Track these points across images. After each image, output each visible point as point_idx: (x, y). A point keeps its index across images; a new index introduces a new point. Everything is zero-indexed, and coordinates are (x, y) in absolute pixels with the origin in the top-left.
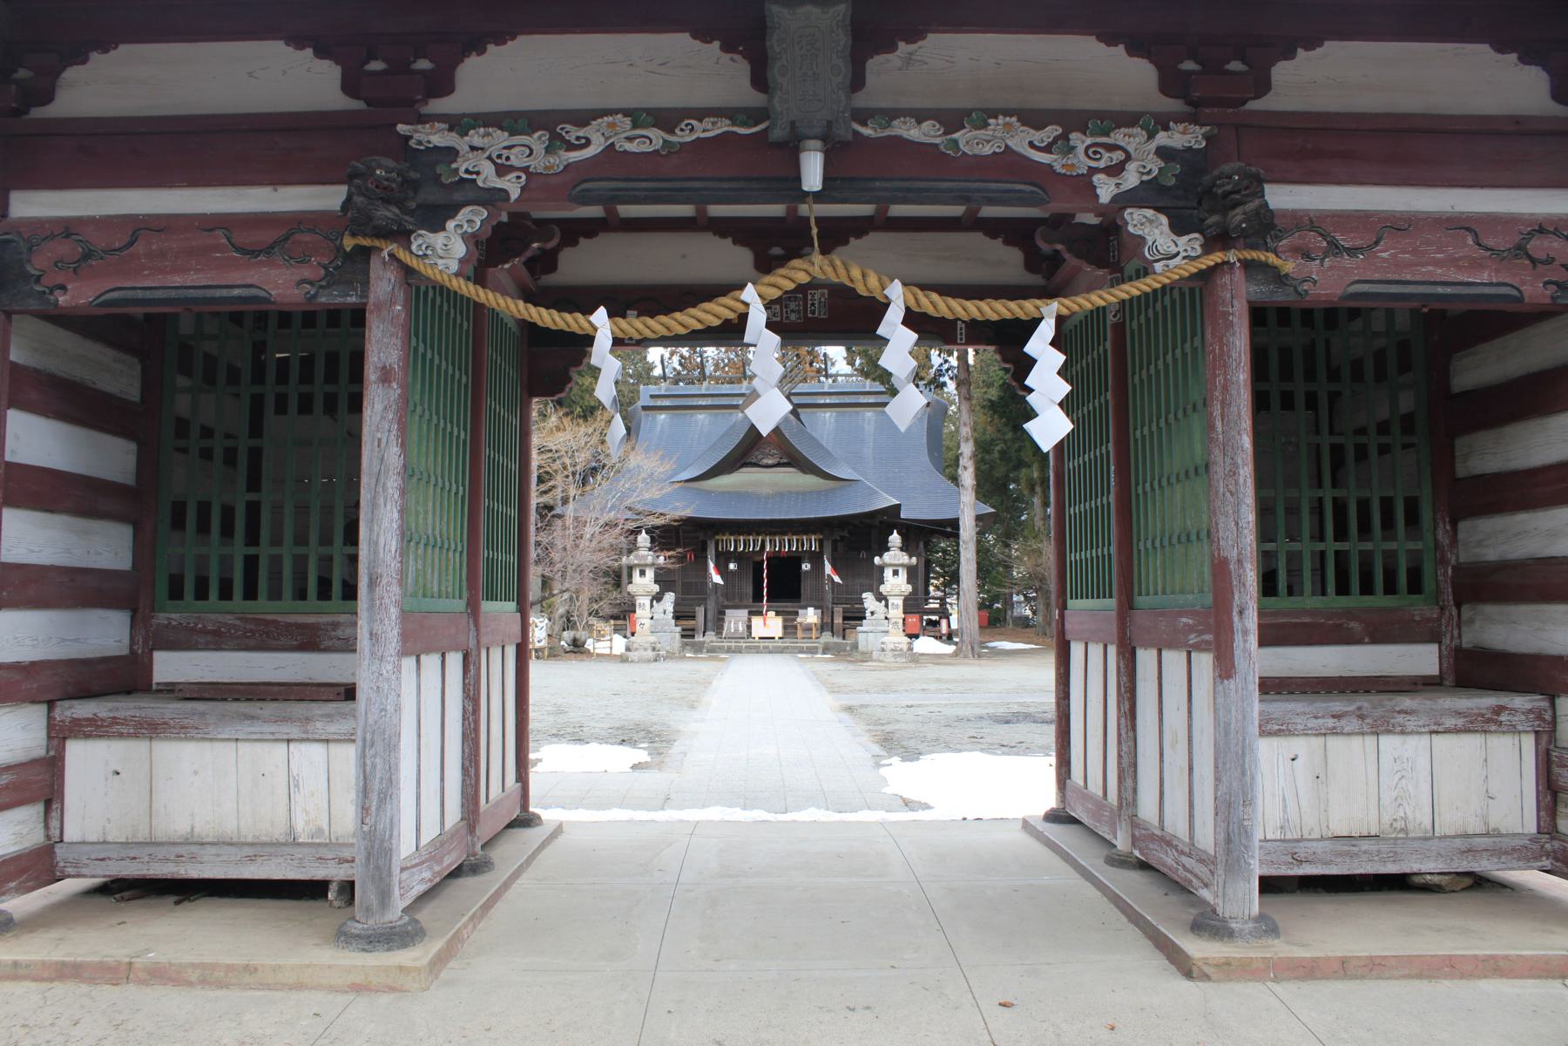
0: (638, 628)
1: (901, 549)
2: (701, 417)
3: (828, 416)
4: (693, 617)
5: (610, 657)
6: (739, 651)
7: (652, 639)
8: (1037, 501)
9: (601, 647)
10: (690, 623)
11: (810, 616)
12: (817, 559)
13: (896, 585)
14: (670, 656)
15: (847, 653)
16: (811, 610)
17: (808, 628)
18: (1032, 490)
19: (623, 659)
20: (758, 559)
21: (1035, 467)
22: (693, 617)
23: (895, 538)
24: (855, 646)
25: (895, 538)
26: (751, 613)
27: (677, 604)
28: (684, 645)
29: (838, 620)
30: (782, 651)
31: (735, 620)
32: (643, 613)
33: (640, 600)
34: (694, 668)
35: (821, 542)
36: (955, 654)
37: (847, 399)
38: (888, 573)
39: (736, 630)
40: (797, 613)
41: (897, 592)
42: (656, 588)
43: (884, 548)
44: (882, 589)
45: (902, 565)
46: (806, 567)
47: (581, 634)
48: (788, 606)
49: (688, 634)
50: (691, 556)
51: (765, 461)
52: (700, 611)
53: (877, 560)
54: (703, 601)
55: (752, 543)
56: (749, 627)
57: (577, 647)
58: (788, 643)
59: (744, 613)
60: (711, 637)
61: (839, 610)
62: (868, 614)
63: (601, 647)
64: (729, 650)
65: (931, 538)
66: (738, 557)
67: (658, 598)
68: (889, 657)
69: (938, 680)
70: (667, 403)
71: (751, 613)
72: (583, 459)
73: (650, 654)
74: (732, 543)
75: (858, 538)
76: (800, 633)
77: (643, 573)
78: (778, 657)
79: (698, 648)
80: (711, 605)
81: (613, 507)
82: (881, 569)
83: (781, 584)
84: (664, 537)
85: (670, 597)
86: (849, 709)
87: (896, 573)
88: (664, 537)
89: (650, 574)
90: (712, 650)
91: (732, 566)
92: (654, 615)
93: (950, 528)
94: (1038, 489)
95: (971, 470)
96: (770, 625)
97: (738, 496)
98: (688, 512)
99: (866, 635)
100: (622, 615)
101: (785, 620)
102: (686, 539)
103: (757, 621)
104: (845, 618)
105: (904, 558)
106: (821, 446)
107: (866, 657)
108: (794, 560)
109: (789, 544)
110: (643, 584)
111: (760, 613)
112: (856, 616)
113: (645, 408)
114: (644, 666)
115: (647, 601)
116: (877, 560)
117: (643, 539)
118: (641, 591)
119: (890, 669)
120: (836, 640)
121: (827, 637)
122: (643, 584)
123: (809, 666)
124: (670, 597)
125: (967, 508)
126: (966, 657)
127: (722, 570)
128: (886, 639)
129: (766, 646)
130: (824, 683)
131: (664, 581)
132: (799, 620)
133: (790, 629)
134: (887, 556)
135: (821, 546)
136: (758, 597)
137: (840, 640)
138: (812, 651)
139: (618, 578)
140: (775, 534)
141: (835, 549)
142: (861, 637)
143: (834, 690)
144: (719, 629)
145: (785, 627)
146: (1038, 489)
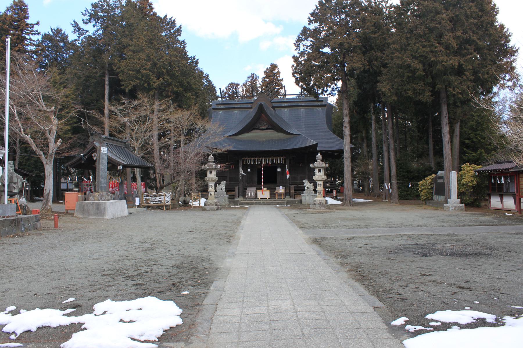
0: (209, 196)
1: (322, 161)
2: (236, 112)
3: (286, 110)
4: (234, 191)
5: (199, 208)
6: (252, 204)
7: (216, 200)
8: (364, 145)
9: (196, 203)
10: (232, 193)
11: (281, 190)
12: (283, 167)
13: (320, 176)
14: (224, 207)
15: (299, 205)
16: (281, 187)
17: (280, 194)
18: (363, 140)
19: (203, 209)
20: (259, 167)
21: (364, 132)
22: (234, 191)
23: (319, 156)
24: (301, 201)
25: (319, 156)
26: (257, 189)
27: (227, 185)
28: (230, 203)
29: (292, 191)
30: (270, 204)
31: (251, 192)
32: (211, 190)
33: (210, 184)
34: (235, 213)
35: (285, 160)
36: (342, 205)
37: (294, 104)
38: (316, 171)
39: (251, 196)
40: (275, 189)
41: (320, 179)
42: (217, 179)
43: (314, 160)
44: (314, 178)
45: (322, 167)
46: (279, 170)
47: (187, 198)
48: (272, 186)
49: (231, 197)
50: (232, 167)
51: (262, 128)
52: (236, 188)
53: (311, 165)
54: (238, 184)
55: (256, 161)
56: (256, 194)
57: (186, 204)
58: (272, 200)
59: (254, 189)
60: (241, 199)
61: (292, 187)
62: (306, 189)
63: (196, 203)
64: (248, 204)
65: (333, 157)
66: (251, 166)
67: (218, 183)
68: (318, 207)
69: (346, 219)
70: (222, 107)
71: (257, 189)
72: (186, 125)
73: (215, 207)
74: (250, 161)
75: (301, 160)
76: (277, 197)
77: (211, 173)
78: (269, 206)
79: (236, 203)
80: (241, 186)
81: (199, 146)
82: (313, 169)
83: (270, 179)
84: (220, 158)
85: (223, 183)
86: (316, 241)
87: (320, 171)
88: (220, 158)
89: (214, 173)
90: (242, 204)
91: (249, 170)
92: (217, 190)
93: (341, 152)
94: (365, 140)
95: (348, 128)
96: (264, 194)
97: (251, 142)
98: (230, 148)
99: (306, 197)
100: (204, 191)
101: (270, 192)
102: (229, 160)
103: (259, 192)
104: (295, 190)
105: (324, 165)
106: (284, 121)
107: (307, 207)
108: (274, 168)
109: (272, 161)
110: (211, 177)
111: (260, 189)
112: (301, 189)
113: (214, 109)
114: (211, 212)
115: (213, 185)
116: (311, 165)
117: (211, 158)
118: (210, 180)
119: (319, 213)
120: (291, 199)
121: (288, 198)
122: (211, 177)
123: (283, 211)
124: (223, 183)
125: (347, 146)
126: (347, 206)
127: (245, 170)
128: (315, 199)
129: (263, 202)
130: (294, 222)
131: (221, 176)
132: (276, 191)
133: (273, 195)
134: (316, 164)
135: (285, 162)
136: (260, 183)
137: (293, 199)
138: (282, 204)
139: (202, 174)
140: (266, 157)
141: (290, 163)
142: (303, 198)
143: (302, 226)
144: (244, 195)
145: (271, 194)
146: (365, 140)
